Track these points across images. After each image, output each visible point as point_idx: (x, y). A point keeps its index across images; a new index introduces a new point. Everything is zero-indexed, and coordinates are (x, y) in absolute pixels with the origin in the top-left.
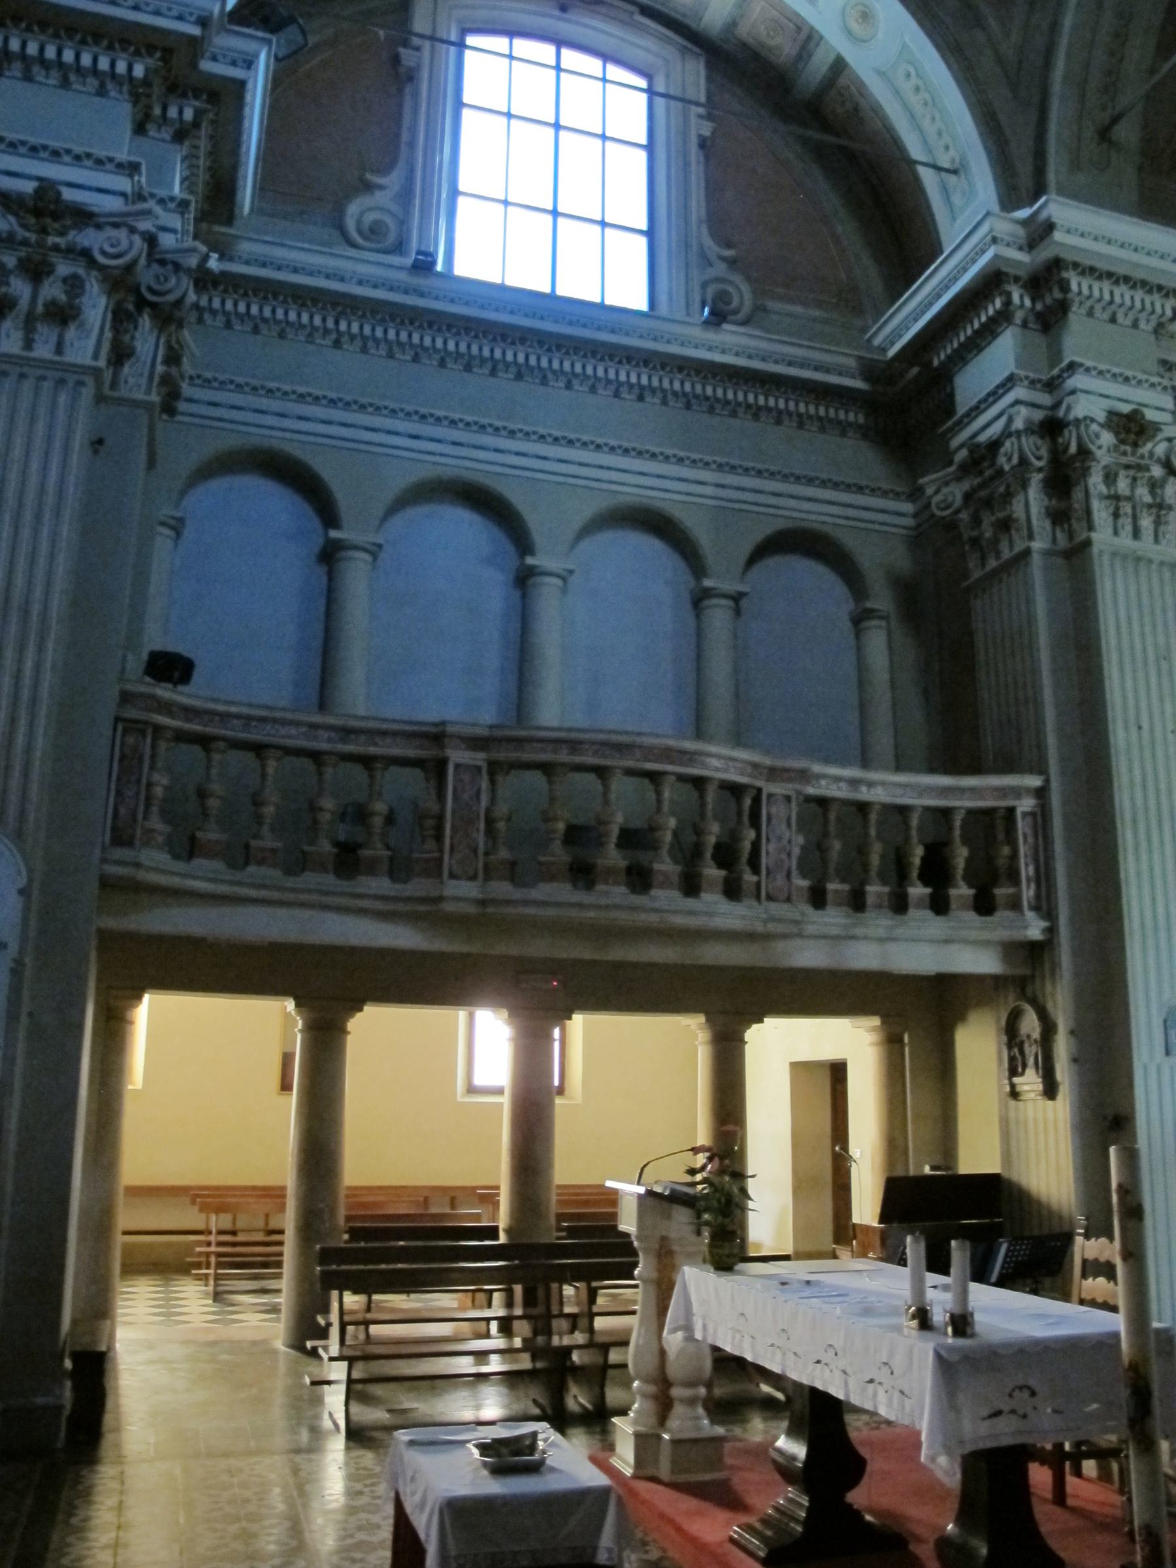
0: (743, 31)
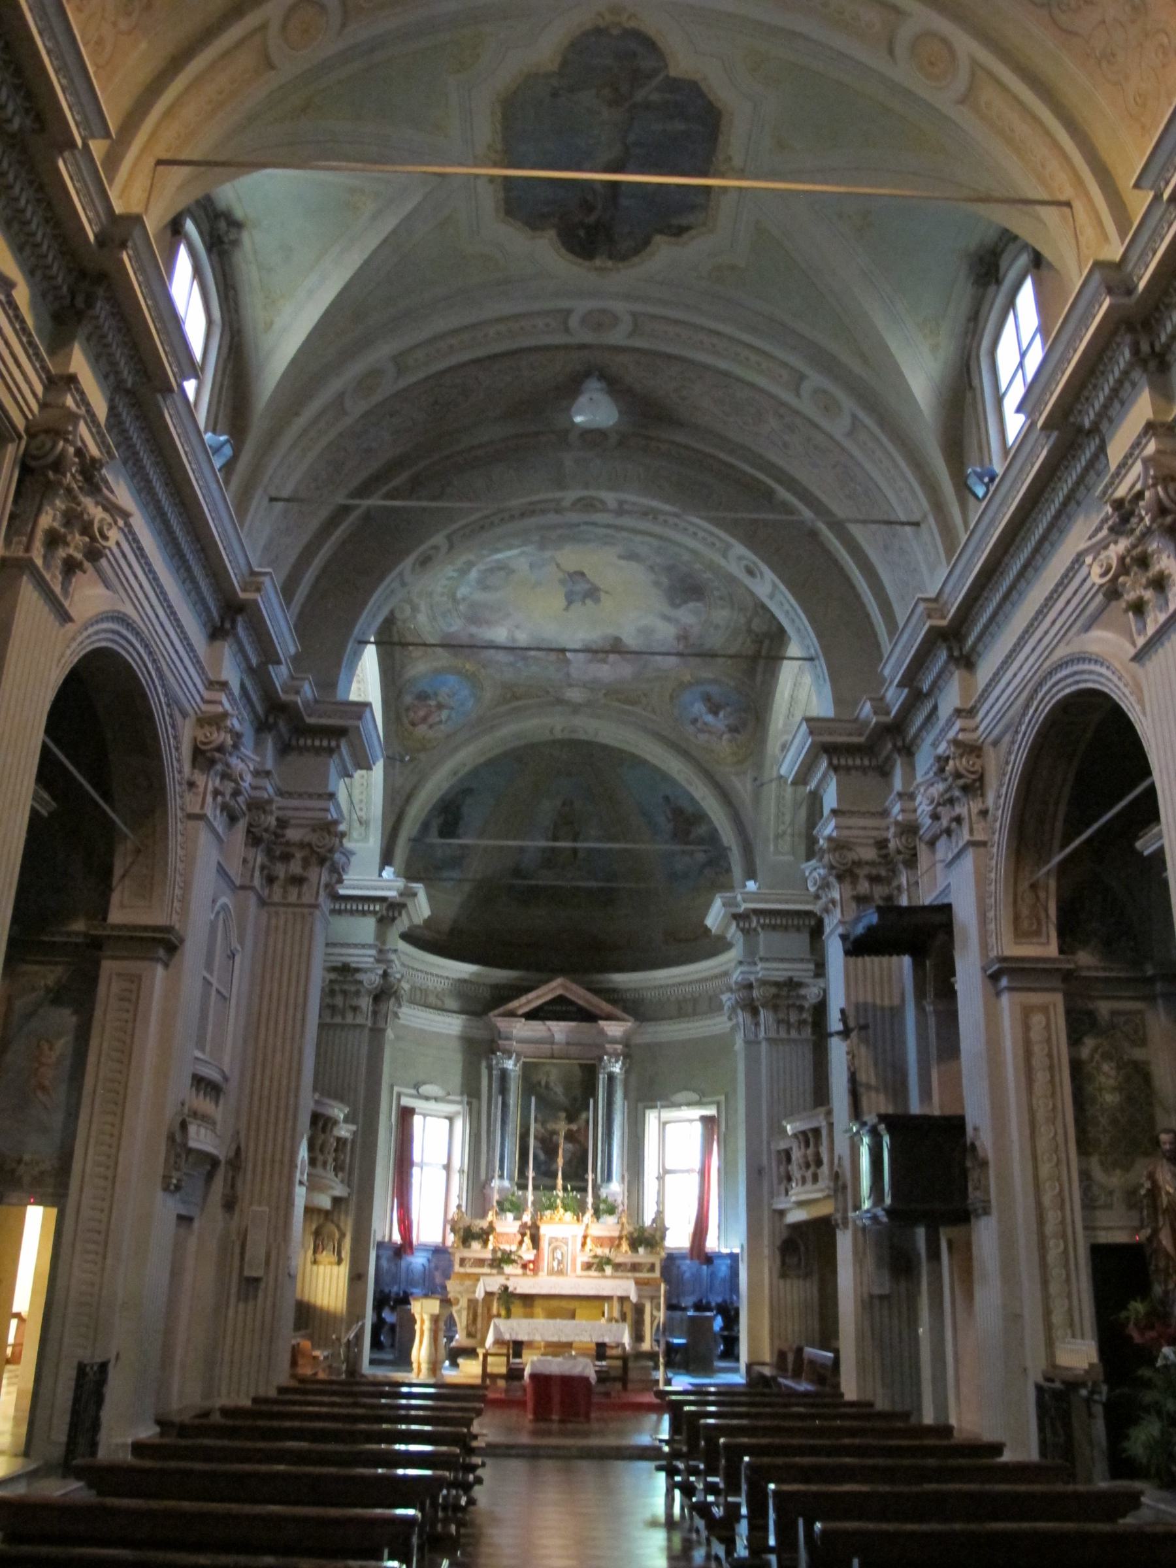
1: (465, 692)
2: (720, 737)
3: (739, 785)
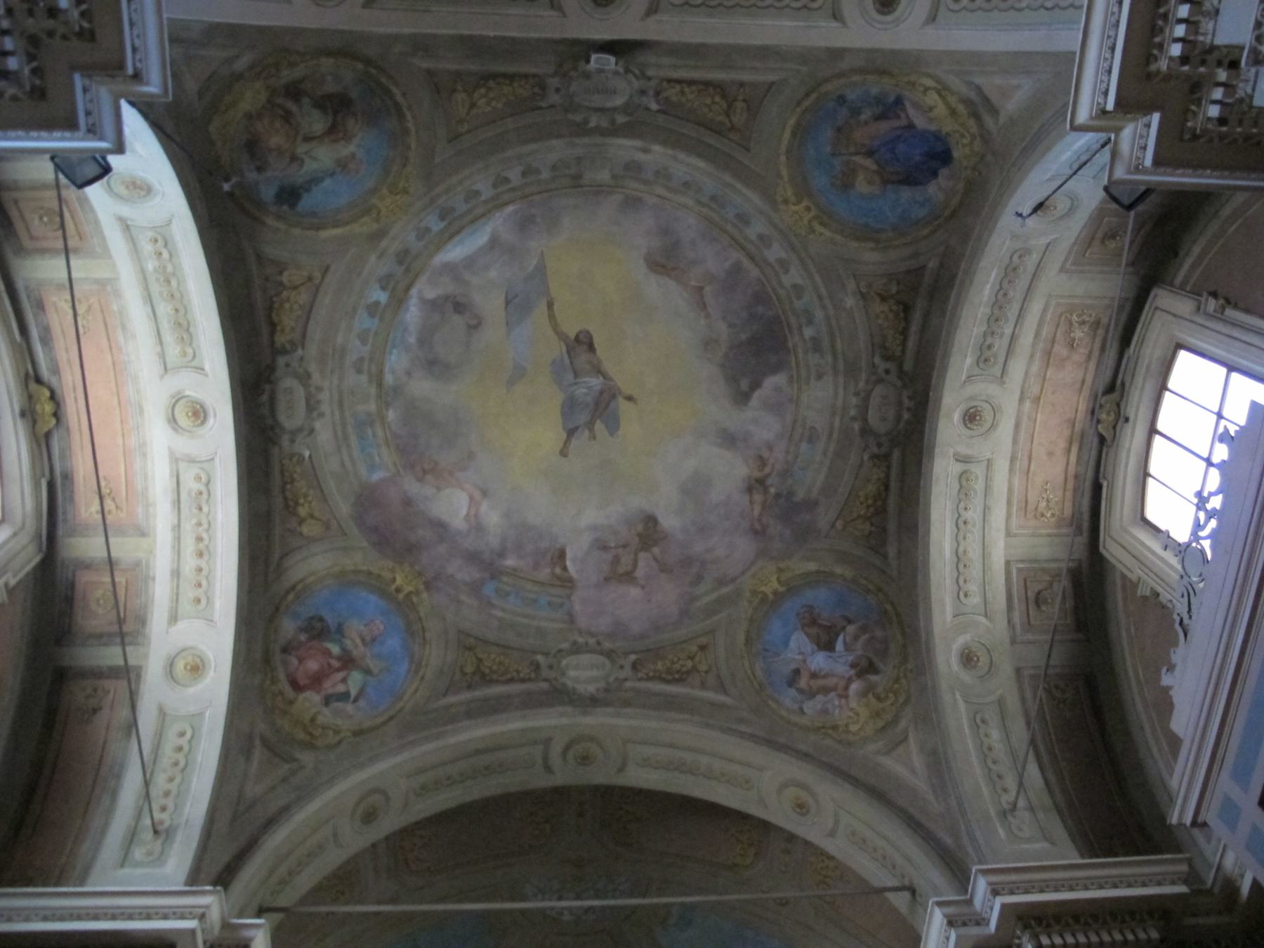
0: (84, 578)
1: (393, 643)
2: (844, 696)
3: (901, 770)
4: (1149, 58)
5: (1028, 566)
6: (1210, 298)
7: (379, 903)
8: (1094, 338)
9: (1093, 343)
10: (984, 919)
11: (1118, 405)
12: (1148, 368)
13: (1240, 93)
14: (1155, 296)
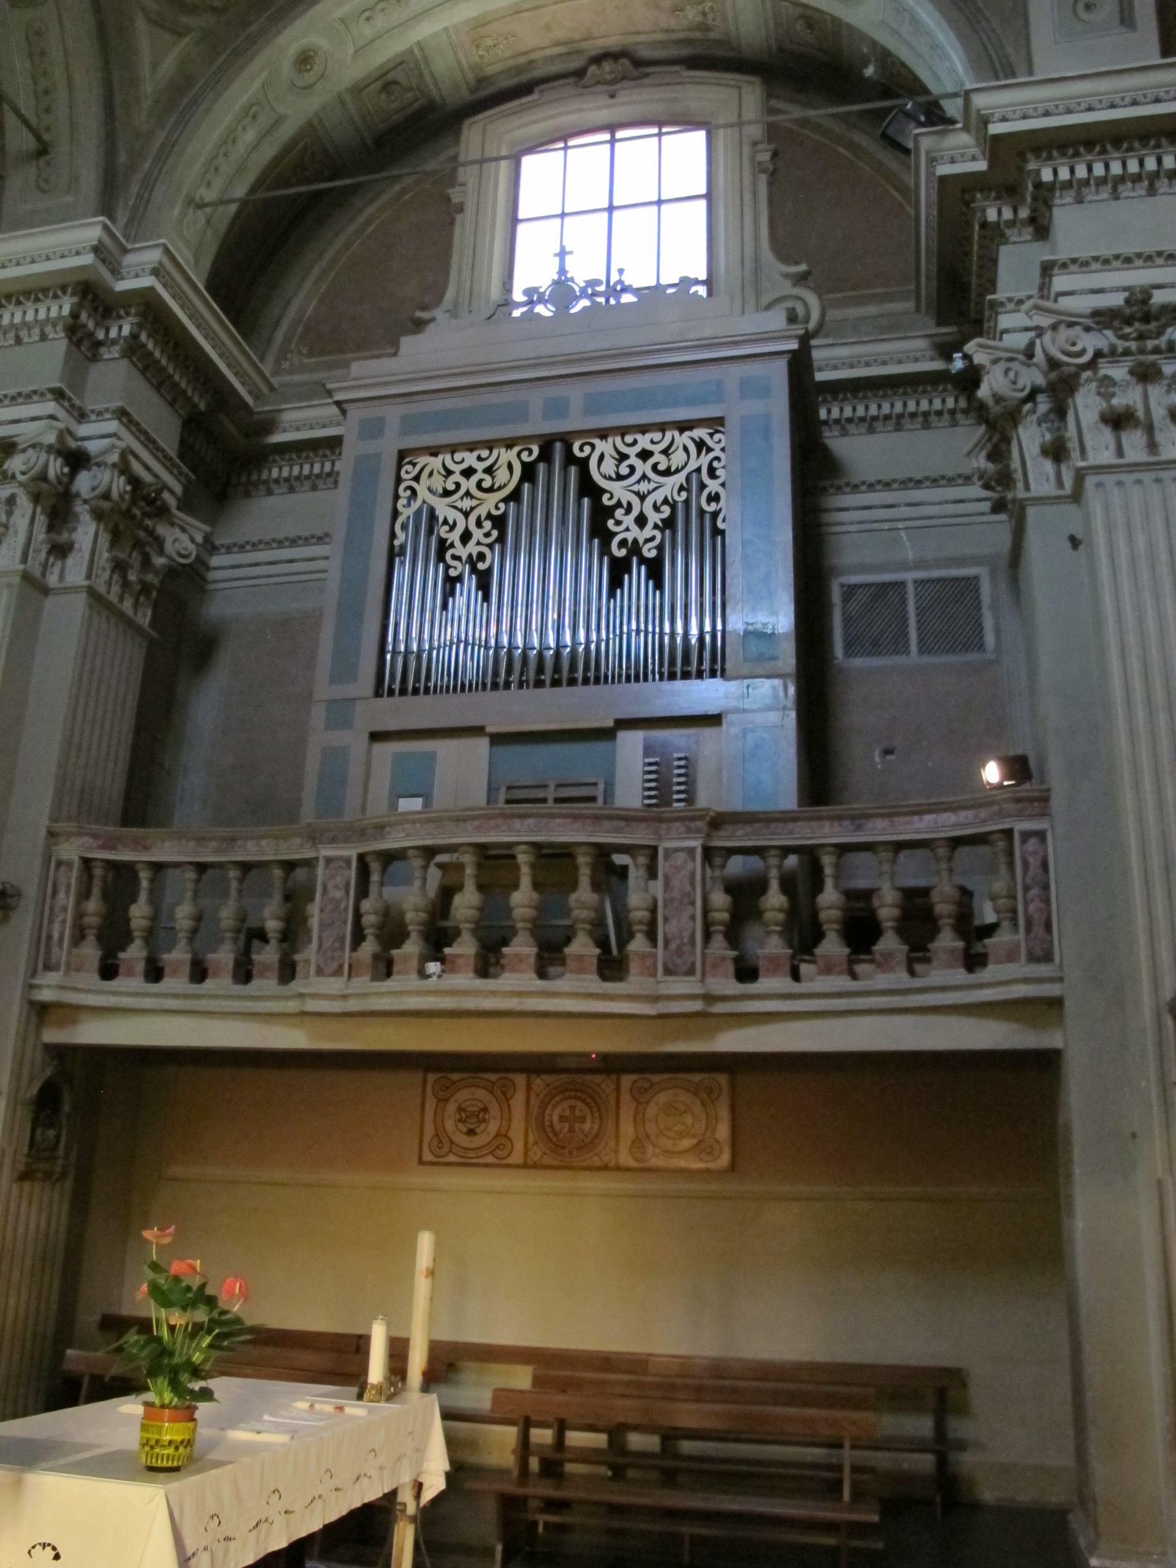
4: (1037, 151)
5: (419, 57)
6: (770, 153)
7: (331, 190)
8: (690, 29)
9: (684, 30)
10: (119, 273)
11: (624, 78)
12: (676, 99)
13: (1008, 232)
14: (751, 83)
